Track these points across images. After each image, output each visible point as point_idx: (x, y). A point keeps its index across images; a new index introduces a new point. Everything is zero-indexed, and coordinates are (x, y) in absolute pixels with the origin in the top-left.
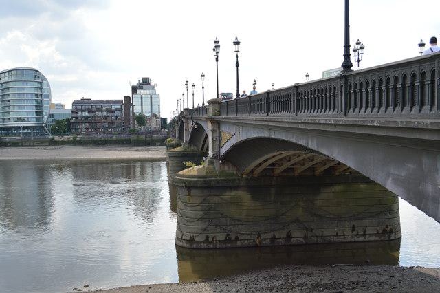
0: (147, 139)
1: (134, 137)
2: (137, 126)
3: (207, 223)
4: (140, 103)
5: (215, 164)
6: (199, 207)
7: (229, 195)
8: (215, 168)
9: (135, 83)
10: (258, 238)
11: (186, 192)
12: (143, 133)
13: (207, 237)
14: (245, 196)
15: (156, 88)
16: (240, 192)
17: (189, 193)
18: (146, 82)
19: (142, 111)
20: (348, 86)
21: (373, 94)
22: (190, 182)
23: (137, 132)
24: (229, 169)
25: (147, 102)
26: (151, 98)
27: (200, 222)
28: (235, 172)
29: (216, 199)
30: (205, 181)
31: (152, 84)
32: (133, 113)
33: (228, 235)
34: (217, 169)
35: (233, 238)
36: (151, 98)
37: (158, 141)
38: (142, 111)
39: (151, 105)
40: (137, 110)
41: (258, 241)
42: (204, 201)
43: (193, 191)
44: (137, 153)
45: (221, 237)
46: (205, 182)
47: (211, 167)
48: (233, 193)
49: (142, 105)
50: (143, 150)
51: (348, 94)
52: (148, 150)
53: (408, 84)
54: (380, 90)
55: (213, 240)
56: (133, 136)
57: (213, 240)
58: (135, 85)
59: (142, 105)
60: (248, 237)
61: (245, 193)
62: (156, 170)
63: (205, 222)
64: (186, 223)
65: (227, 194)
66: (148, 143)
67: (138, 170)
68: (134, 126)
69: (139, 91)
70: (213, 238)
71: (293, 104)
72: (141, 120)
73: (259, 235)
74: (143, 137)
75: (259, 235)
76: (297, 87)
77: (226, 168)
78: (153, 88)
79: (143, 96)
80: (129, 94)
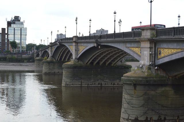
0: (18, 57)
1: (9, 56)
2: (11, 49)
3: (147, 109)
4: (13, 33)
5: (152, 70)
6: (142, 98)
7: (160, 90)
8: (152, 72)
9: (9, 20)
10: (178, 118)
11: (132, 87)
12: (15, 54)
13: (147, 118)
14: (169, 90)
15: (24, 24)
16: (168, 88)
17: (135, 88)
18: (17, 19)
19: (14, 39)
20: (174, 31)
21: (181, 32)
22: (136, 81)
23: (8, 52)
24: (161, 73)
25: (18, 32)
26: (21, 30)
27: (142, 108)
28: (165, 76)
29: (153, 93)
30: (147, 80)
31: (21, 21)
32: (8, 40)
33: (159, 117)
34: (153, 73)
35: (163, 119)
36: (21, 30)
37: (26, 59)
38: (14, 39)
39: (21, 35)
40: (11, 38)
41: (178, 120)
42: (145, 94)
43: (138, 87)
44: (14, 67)
45: (155, 118)
46: (147, 81)
47: (150, 71)
48: (163, 89)
49: (14, 34)
50: (18, 65)
51: (174, 32)
52: (21, 65)
53: (177, 31)
54: (168, 32)
55: (151, 120)
56: (8, 55)
57: (151, 120)
58: (10, 21)
59: (14, 34)
60: (172, 118)
61: (170, 89)
62: (22, 78)
63: (146, 107)
64: (131, 108)
65: (159, 90)
66: (19, 61)
67: (10, 78)
68: (8, 48)
69: (12, 25)
70: (151, 118)
71: (114, 37)
72: (14, 44)
73: (178, 117)
74: (16, 56)
75: (178, 117)
76: (174, 28)
77: (159, 72)
78: (22, 23)
79: (16, 29)
80: (5, 26)
